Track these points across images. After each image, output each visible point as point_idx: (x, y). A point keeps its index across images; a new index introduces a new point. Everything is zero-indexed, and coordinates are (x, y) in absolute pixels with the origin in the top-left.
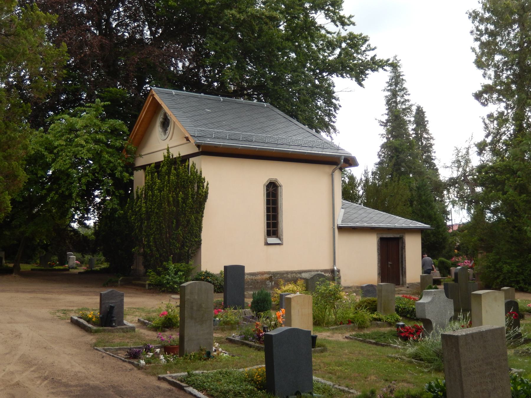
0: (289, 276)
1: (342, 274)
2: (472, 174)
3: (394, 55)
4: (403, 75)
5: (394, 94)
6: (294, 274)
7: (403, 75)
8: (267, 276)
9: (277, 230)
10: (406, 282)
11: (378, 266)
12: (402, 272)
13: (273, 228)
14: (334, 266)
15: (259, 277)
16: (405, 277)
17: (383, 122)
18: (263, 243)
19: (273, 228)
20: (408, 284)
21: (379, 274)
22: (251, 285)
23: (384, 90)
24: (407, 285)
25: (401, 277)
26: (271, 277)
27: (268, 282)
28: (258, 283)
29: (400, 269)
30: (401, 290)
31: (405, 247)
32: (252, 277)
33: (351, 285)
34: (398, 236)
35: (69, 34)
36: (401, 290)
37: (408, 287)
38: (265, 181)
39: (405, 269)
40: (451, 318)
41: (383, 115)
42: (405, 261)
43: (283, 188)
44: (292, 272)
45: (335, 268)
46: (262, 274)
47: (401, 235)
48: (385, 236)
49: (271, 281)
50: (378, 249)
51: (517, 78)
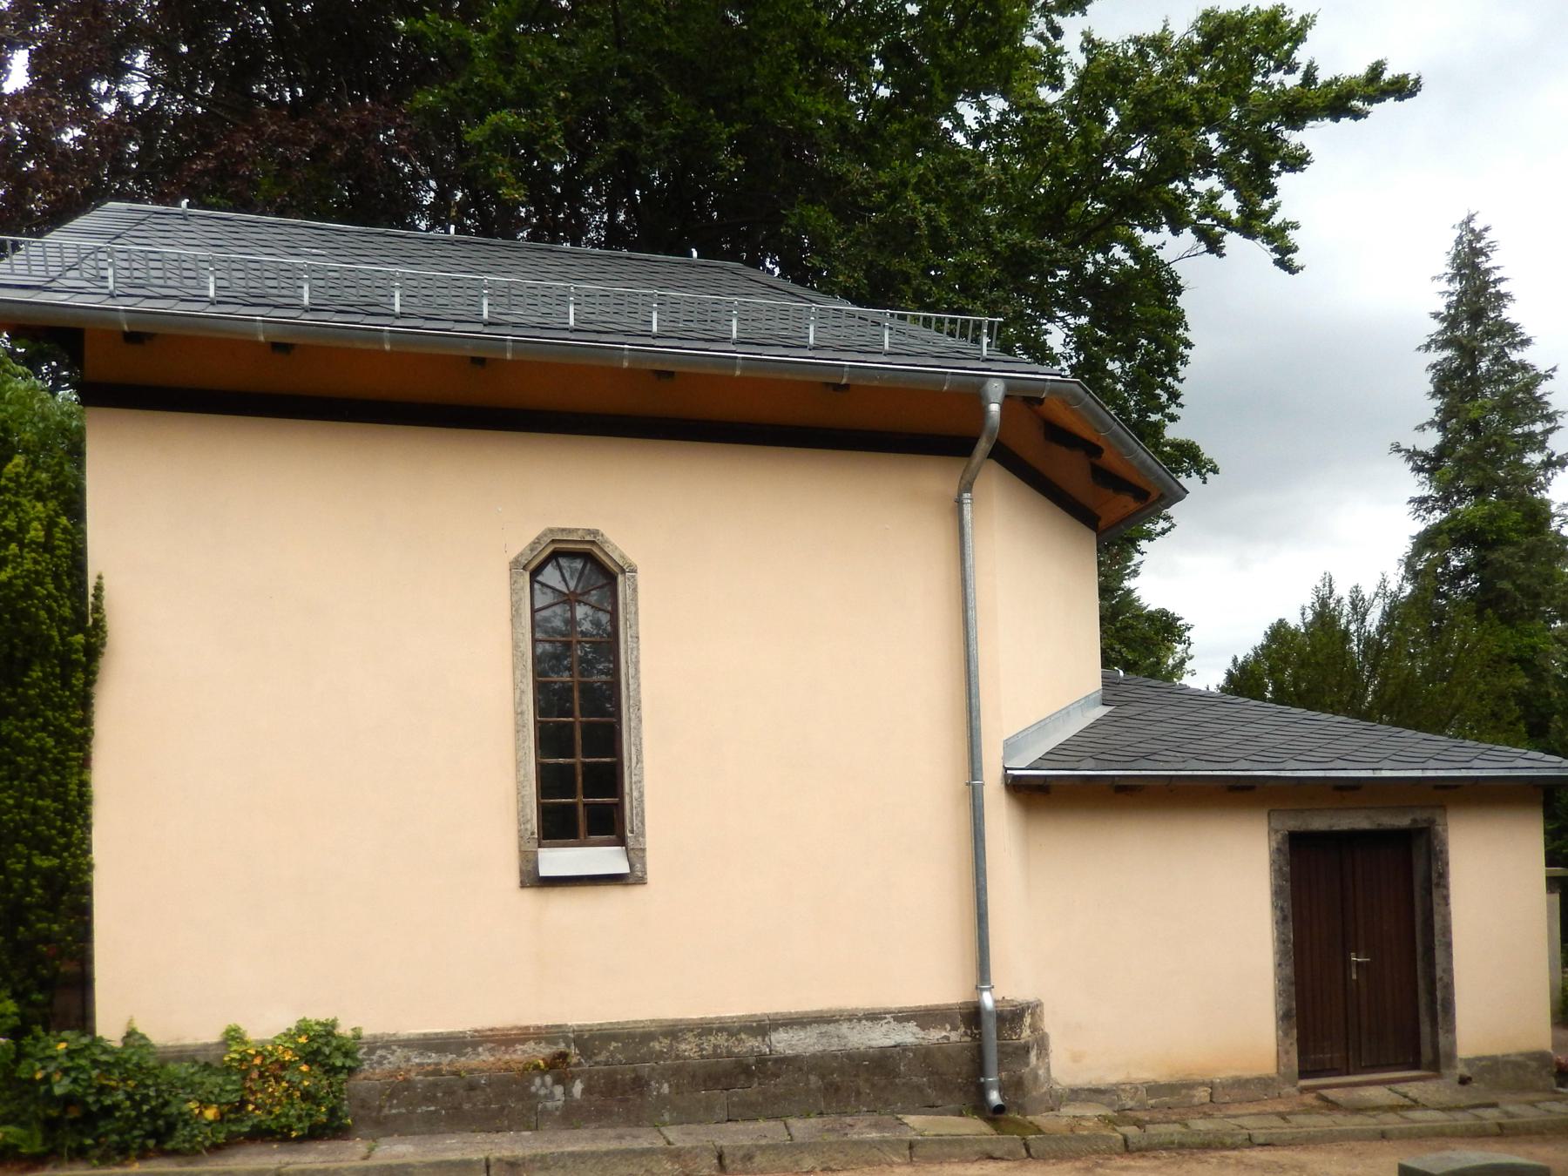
0: (688, 1048)
3: (1464, 217)
4: (1501, 280)
5: (1468, 352)
7: (1501, 280)
8: (540, 1052)
9: (620, 806)
10: (1451, 1055)
11: (1281, 979)
12: (1433, 1001)
14: (979, 990)
16: (1451, 1029)
17: (1426, 457)
18: (514, 878)
20: (1469, 1062)
21: (1284, 1018)
23: (1428, 347)
24: (1462, 1070)
25: (1425, 1029)
26: (563, 1056)
28: (472, 1087)
29: (1421, 984)
30: (1415, 1104)
31: (1443, 876)
32: (434, 1057)
33: (1111, 1078)
34: (1404, 821)
36: (1415, 1104)
37: (1464, 1081)
38: (522, 536)
39: (1449, 987)
40: (1412, 94)
41: (1421, 428)
42: (1448, 945)
43: (642, 578)
44: (705, 1029)
45: (988, 1000)
47: (1422, 815)
48: (1319, 823)
49: (563, 1080)
50: (1277, 893)
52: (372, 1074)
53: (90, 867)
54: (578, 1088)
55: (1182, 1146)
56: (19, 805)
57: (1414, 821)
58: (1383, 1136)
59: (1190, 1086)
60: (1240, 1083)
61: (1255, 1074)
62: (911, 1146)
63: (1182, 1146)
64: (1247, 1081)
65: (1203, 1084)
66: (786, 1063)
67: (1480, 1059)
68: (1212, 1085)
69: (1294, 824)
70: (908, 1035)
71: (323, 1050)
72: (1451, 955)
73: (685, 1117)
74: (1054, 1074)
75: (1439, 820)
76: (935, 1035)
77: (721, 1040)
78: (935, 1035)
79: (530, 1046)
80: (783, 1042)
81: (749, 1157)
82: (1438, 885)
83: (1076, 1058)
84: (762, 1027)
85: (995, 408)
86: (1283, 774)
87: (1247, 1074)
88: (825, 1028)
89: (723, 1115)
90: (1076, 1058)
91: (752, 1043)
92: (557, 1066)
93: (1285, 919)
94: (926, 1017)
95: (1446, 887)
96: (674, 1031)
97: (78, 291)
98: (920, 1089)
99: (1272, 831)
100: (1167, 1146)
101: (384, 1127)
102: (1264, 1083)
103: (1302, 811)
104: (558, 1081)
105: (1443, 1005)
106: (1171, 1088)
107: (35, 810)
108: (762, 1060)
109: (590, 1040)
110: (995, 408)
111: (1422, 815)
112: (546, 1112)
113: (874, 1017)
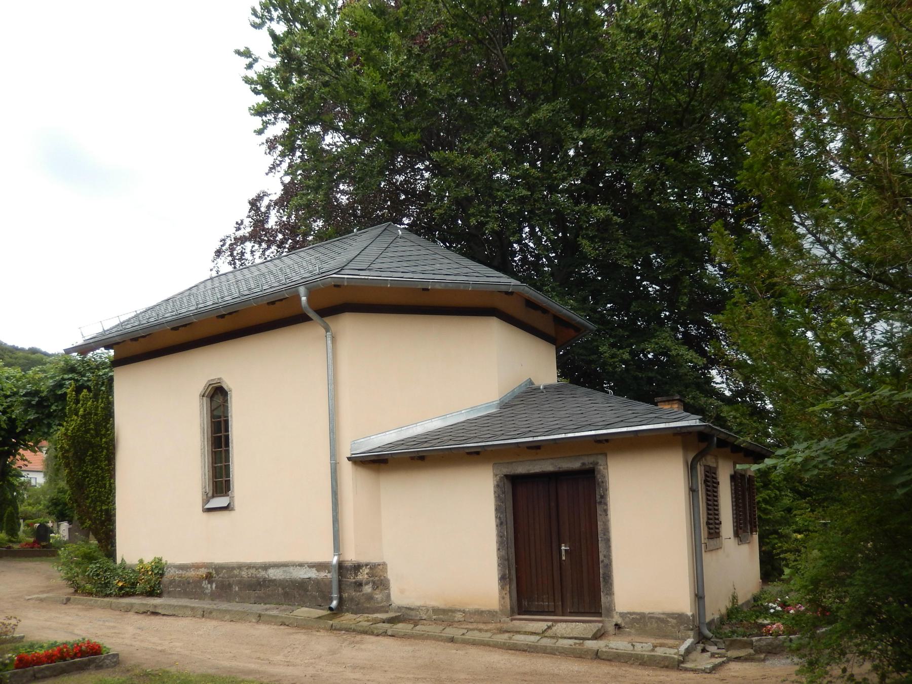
1: (391, 575)
2: (585, 300)
6: (253, 571)
8: (203, 572)
13: (220, 481)
15: (192, 573)
16: (610, 593)
19: (220, 481)
20: (622, 615)
22: (179, 586)
24: (617, 619)
27: (205, 584)
28: (189, 583)
32: (181, 572)
34: (576, 465)
35: (430, 222)
42: (608, 541)
44: (249, 567)
46: (197, 567)
47: (592, 459)
49: (210, 582)
50: (498, 509)
51: (520, 154)
52: (169, 574)
53: (115, 509)
54: (214, 586)
55: (354, 631)
56: (95, 491)
57: (583, 464)
58: (452, 640)
59: (453, 611)
60: (480, 613)
61: (488, 608)
62: (260, 616)
63: (354, 631)
64: (482, 612)
65: (460, 611)
66: (273, 582)
67: (631, 614)
68: (464, 612)
69: (506, 470)
70: (313, 574)
71: (159, 569)
72: (610, 547)
73: (243, 600)
74: (393, 597)
75: (600, 462)
76: (323, 574)
77: (253, 571)
78: (323, 574)
79: (203, 569)
80: (273, 574)
81: (211, 613)
82: (600, 503)
83: (402, 591)
84: (266, 567)
85: (304, 299)
86: (536, 439)
87: (484, 609)
88: (285, 569)
89: (253, 601)
90: (402, 591)
91: (262, 573)
92: (209, 577)
93: (501, 524)
94: (320, 566)
95: (606, 504)
96: (240, 567)
97: (380, 270)
98: (315, 597)
99: (495, 475)
100: (348, 630)
101: (170, 594)
102: (492, 614)
103: (512, 463)
104: (209, 583)
105: (604, 578)
106: (444, 611)
107: (100, 492)
108: (265, 580)
109: (219, 568)
110: (304, 299)
111: (588, 461)
112: (205, 594)
113: (301, 565)
